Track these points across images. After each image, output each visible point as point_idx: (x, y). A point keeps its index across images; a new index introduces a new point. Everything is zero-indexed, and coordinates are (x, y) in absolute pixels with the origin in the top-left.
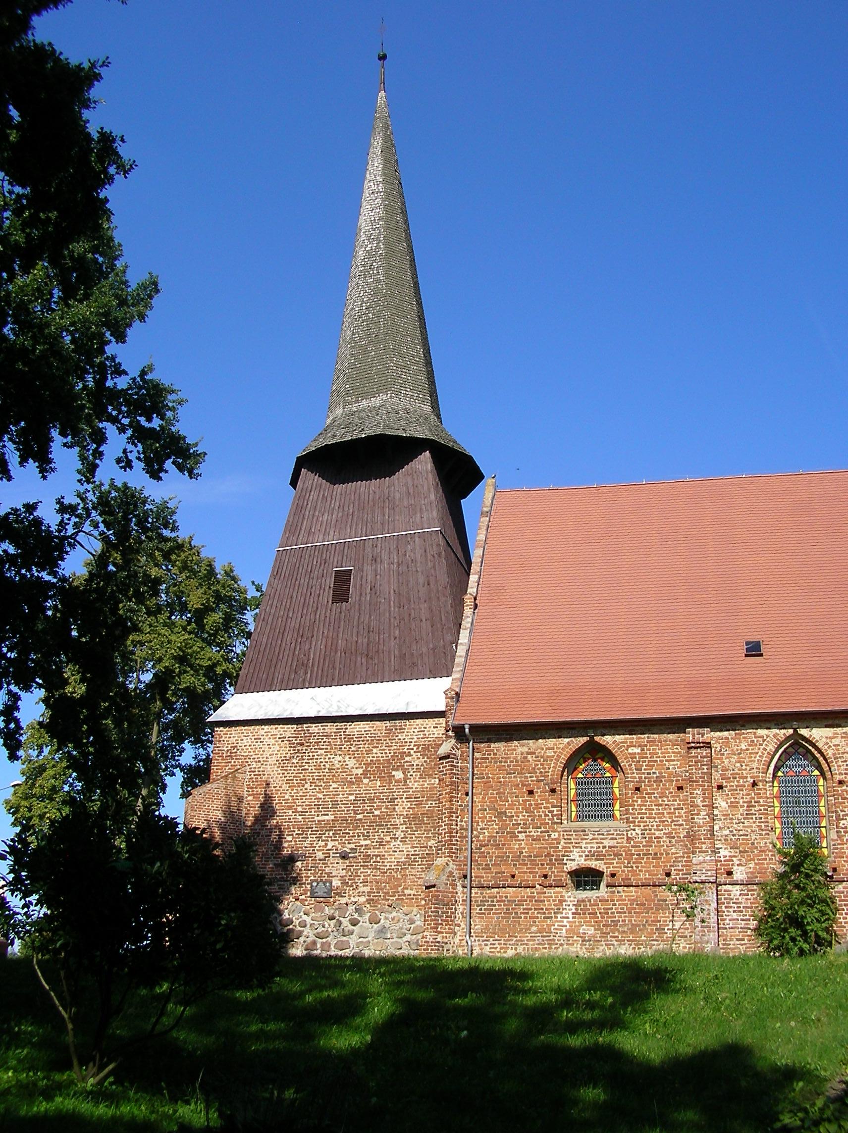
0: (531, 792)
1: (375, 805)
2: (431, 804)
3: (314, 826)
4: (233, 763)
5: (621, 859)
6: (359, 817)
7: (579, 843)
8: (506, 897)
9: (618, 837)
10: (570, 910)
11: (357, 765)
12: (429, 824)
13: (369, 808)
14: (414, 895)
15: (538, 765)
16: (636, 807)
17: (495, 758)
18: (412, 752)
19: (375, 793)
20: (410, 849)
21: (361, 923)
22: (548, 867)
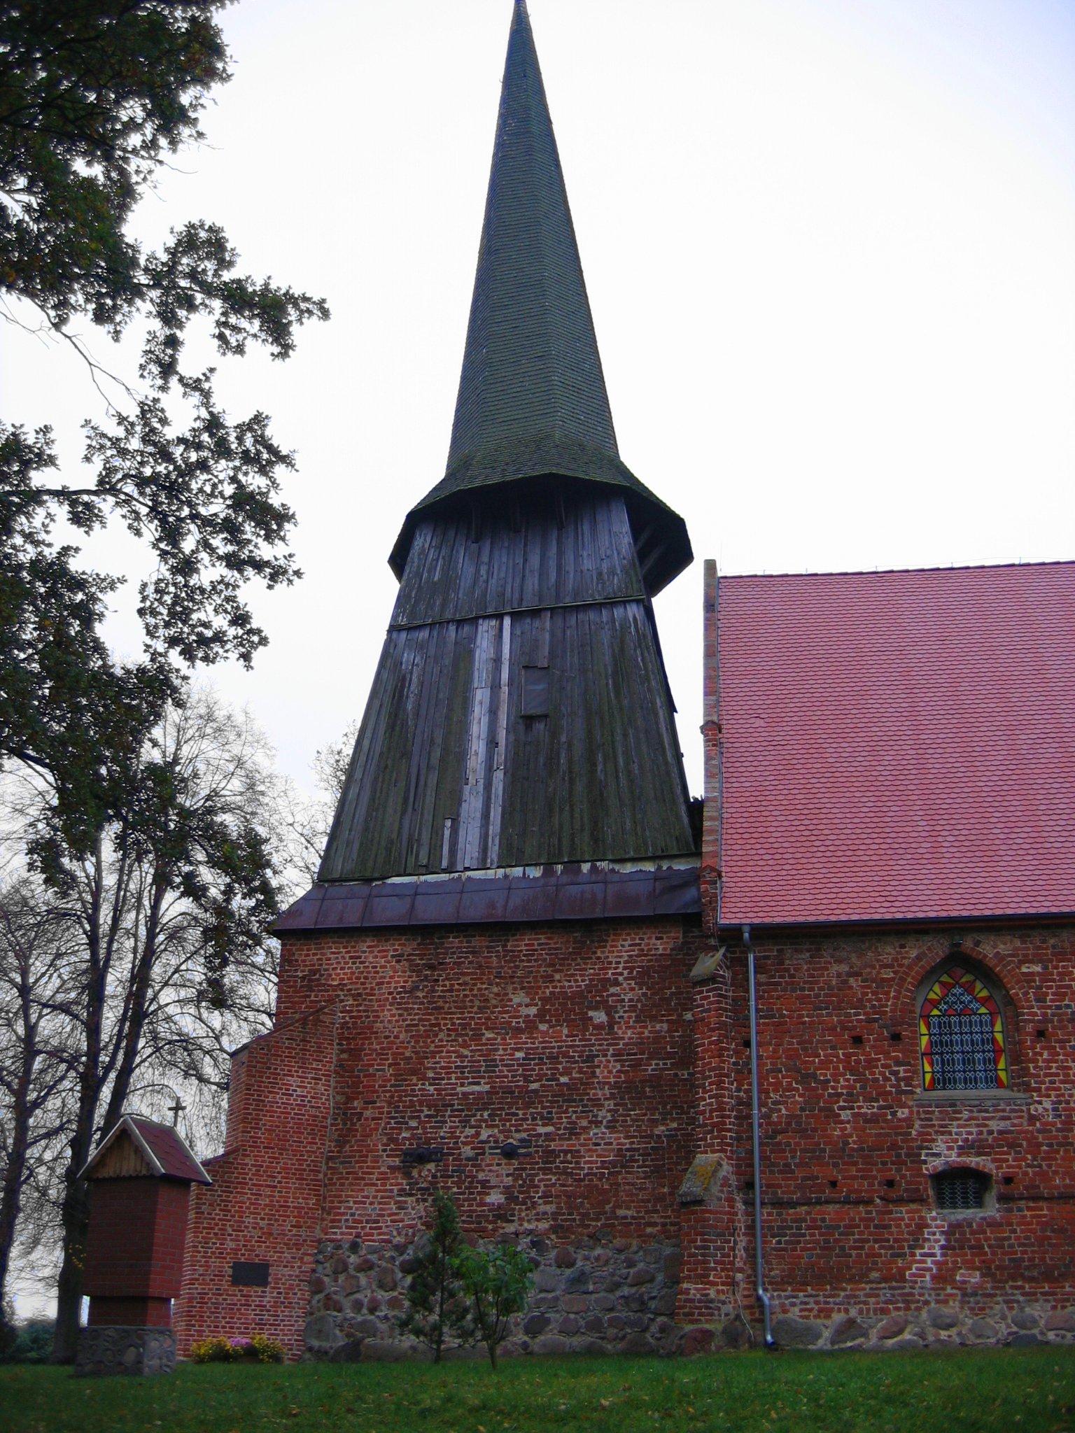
0: (858, 1040)
1: (560, 1066)
2: (657, 1064)
3: (456, 1102)
4: (312, 998)
5: (1020, 1152)
6: (534, 1086)
7: (946, 1126)
8: (823, 1220)
9: (1013, 1115)
10: (937, 1241)
11: (528, 1000)
12: (654, 1097)
13: (549, 1072)
14: (633, 1217)
15: (867, 994)
16: (1040, 1064)
17: (793, 983)
18: (621, 978)
19: (559, 1047)
20: (623, 1140)
21: (542, 1267)
22: (894, 1167)
